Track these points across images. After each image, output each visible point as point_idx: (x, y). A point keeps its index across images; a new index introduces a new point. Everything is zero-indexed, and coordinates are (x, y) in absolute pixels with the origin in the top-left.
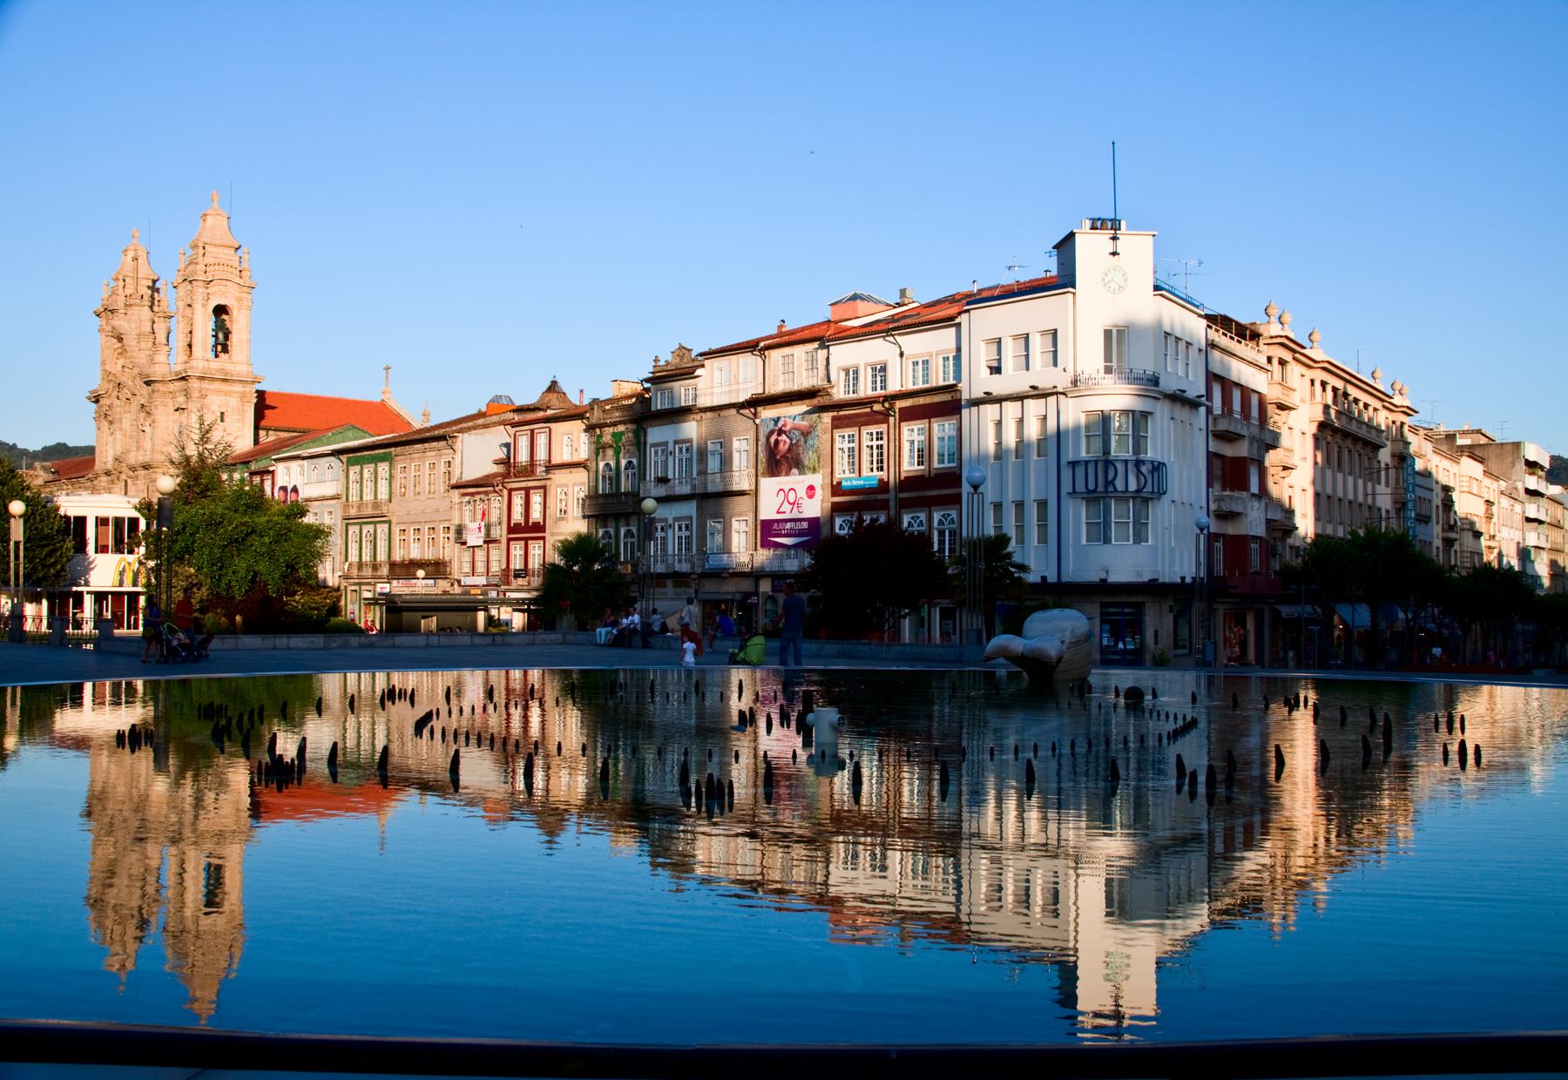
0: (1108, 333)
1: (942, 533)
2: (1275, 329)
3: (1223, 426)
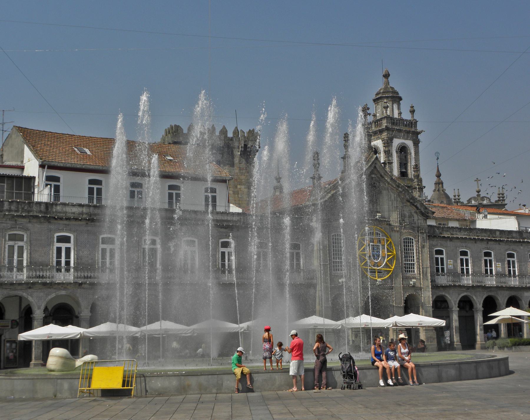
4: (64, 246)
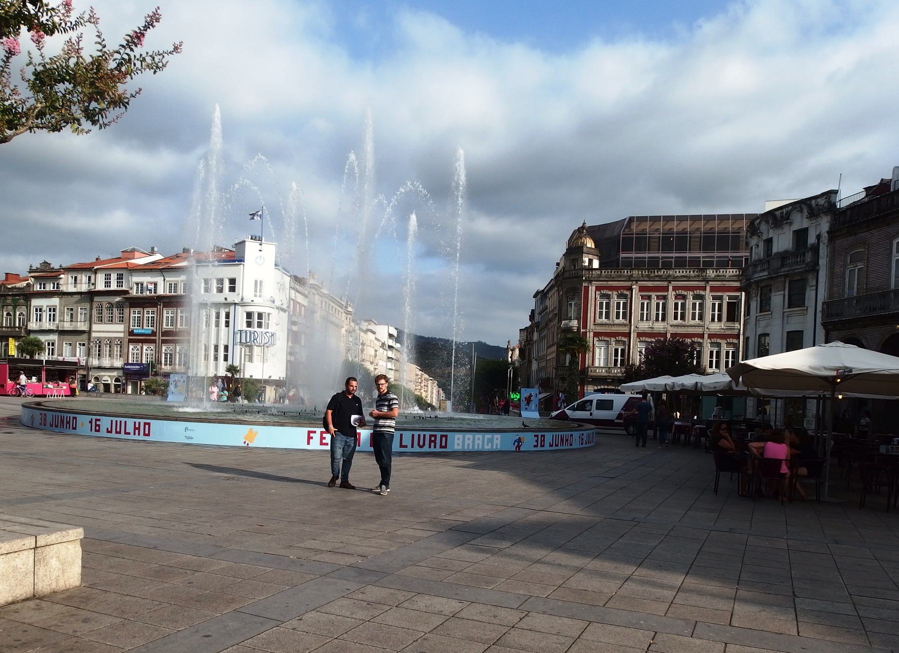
0: (256, 282)
1: (166, 355)
2: (312, 281)
3: (295, 319)
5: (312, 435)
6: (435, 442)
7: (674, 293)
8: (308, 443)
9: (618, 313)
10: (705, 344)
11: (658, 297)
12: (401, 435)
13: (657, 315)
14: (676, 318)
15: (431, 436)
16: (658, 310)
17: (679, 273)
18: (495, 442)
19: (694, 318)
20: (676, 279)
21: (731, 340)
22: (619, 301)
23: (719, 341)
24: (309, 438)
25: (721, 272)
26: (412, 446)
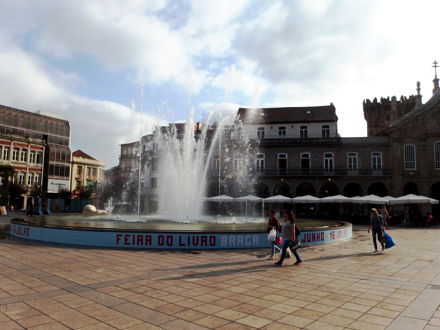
4: (329, 159)
5: (119, 237)
6: (206, 241)
7: (14, 146)
8: (117, 243)
9: (22, 158)
10: (27, 173)
11: (5, 147)
12: (180, 237)
13: (5, 156)
14: (14, 159)
15: (139, 236)
16: (5, 154)
17: (17, 137)
18: (254, 240)
19: (22, 160)
20: (15, 140)
21: (23, 170)
22: (23, 152)
23: (33, 172)
24: (118, 239)
25: (35, 140)
26: (189, 245)
